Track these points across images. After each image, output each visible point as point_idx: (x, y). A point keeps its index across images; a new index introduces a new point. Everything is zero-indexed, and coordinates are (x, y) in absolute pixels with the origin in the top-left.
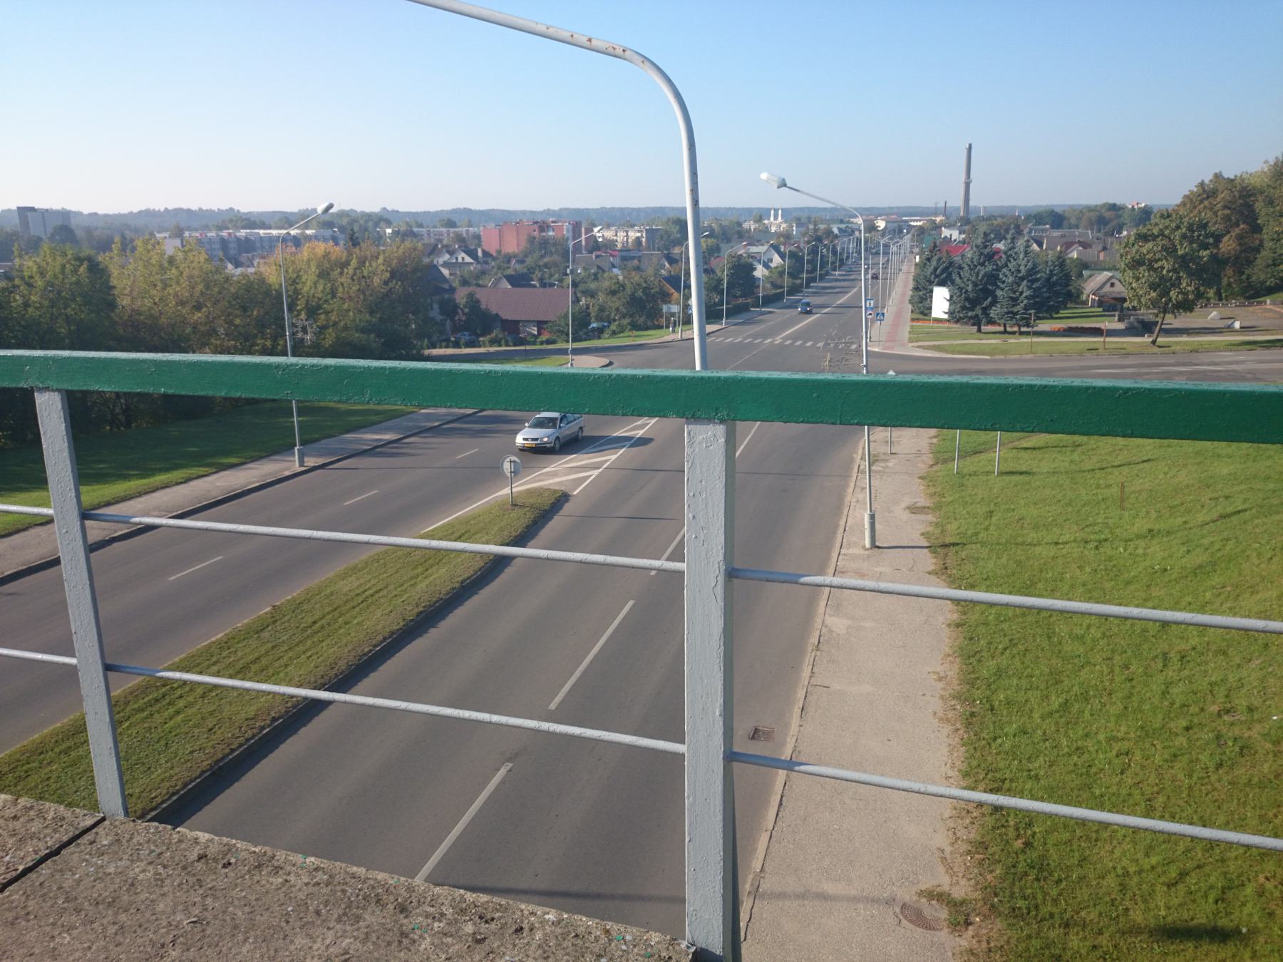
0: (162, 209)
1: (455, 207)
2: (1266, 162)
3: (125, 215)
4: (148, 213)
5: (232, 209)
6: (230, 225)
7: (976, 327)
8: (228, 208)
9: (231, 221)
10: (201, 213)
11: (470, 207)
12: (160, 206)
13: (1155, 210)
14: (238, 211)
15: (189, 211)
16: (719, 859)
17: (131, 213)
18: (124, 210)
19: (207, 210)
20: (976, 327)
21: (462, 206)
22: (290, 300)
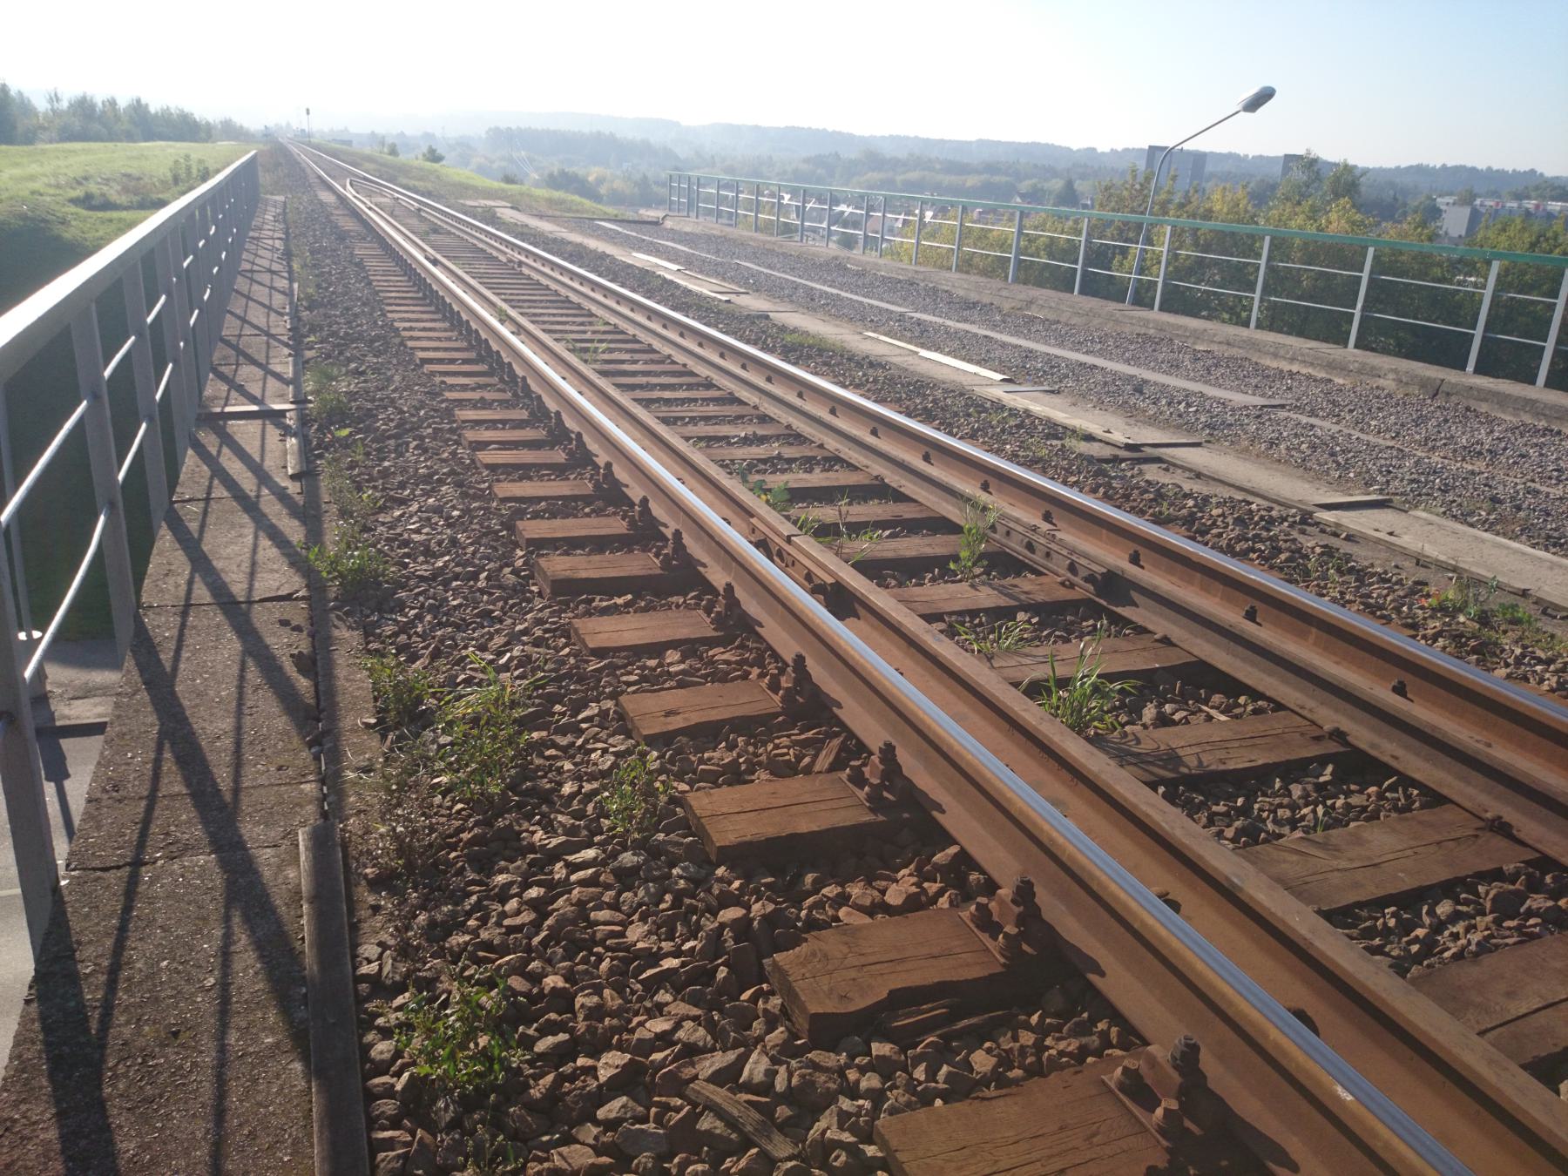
0: (1438, 166)
1: (837, 129)
2: (55, 98)
3: (1390, 170)
4: (1419, 170)
5: (1533, 172)
6: (1533, 194)
7: (380, 950)
8: (1527, 169)
9: (1537, 188)
10: (1500, 176)
11: (1469, 163)
12: (1057, 144)
13: (1413, 203)
14: (1541, 175)
15: (1474, 170)
16: (122, 1028)
17: (1398, 168)
18: (1390, 164)
19: (1497, 171)
20: (380, 950)
21: (1414, 163)
22: (1294, 272)
